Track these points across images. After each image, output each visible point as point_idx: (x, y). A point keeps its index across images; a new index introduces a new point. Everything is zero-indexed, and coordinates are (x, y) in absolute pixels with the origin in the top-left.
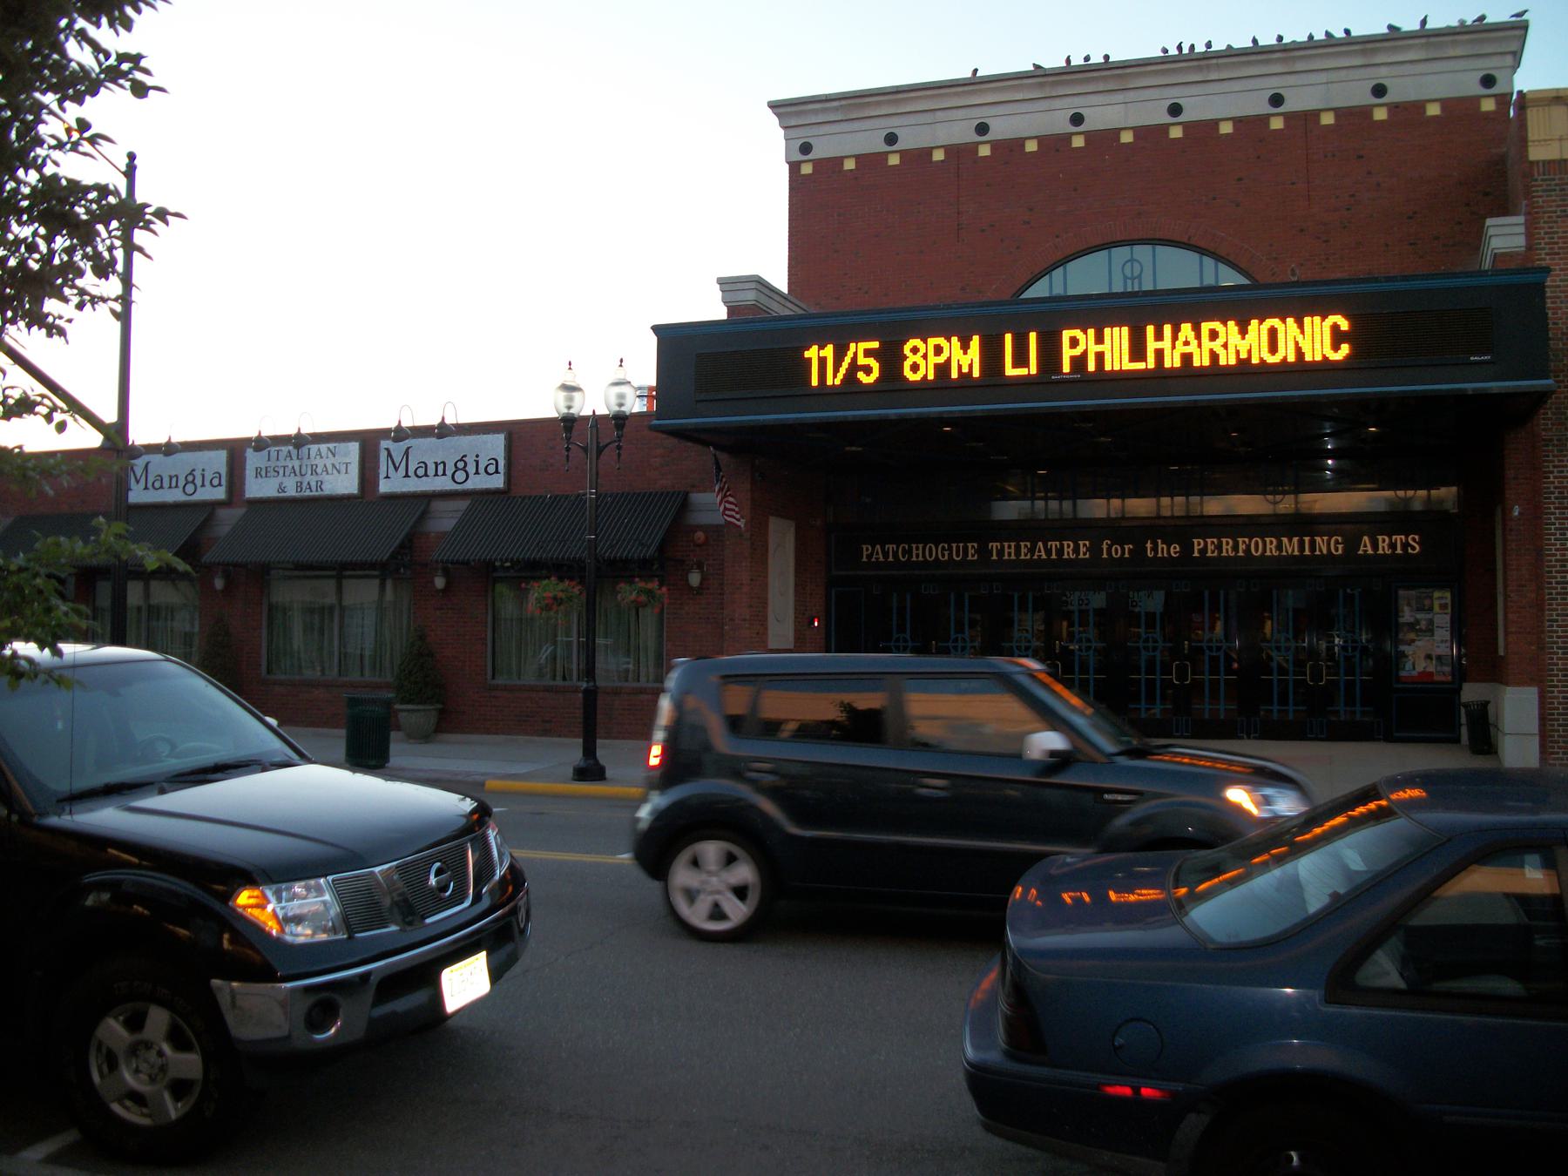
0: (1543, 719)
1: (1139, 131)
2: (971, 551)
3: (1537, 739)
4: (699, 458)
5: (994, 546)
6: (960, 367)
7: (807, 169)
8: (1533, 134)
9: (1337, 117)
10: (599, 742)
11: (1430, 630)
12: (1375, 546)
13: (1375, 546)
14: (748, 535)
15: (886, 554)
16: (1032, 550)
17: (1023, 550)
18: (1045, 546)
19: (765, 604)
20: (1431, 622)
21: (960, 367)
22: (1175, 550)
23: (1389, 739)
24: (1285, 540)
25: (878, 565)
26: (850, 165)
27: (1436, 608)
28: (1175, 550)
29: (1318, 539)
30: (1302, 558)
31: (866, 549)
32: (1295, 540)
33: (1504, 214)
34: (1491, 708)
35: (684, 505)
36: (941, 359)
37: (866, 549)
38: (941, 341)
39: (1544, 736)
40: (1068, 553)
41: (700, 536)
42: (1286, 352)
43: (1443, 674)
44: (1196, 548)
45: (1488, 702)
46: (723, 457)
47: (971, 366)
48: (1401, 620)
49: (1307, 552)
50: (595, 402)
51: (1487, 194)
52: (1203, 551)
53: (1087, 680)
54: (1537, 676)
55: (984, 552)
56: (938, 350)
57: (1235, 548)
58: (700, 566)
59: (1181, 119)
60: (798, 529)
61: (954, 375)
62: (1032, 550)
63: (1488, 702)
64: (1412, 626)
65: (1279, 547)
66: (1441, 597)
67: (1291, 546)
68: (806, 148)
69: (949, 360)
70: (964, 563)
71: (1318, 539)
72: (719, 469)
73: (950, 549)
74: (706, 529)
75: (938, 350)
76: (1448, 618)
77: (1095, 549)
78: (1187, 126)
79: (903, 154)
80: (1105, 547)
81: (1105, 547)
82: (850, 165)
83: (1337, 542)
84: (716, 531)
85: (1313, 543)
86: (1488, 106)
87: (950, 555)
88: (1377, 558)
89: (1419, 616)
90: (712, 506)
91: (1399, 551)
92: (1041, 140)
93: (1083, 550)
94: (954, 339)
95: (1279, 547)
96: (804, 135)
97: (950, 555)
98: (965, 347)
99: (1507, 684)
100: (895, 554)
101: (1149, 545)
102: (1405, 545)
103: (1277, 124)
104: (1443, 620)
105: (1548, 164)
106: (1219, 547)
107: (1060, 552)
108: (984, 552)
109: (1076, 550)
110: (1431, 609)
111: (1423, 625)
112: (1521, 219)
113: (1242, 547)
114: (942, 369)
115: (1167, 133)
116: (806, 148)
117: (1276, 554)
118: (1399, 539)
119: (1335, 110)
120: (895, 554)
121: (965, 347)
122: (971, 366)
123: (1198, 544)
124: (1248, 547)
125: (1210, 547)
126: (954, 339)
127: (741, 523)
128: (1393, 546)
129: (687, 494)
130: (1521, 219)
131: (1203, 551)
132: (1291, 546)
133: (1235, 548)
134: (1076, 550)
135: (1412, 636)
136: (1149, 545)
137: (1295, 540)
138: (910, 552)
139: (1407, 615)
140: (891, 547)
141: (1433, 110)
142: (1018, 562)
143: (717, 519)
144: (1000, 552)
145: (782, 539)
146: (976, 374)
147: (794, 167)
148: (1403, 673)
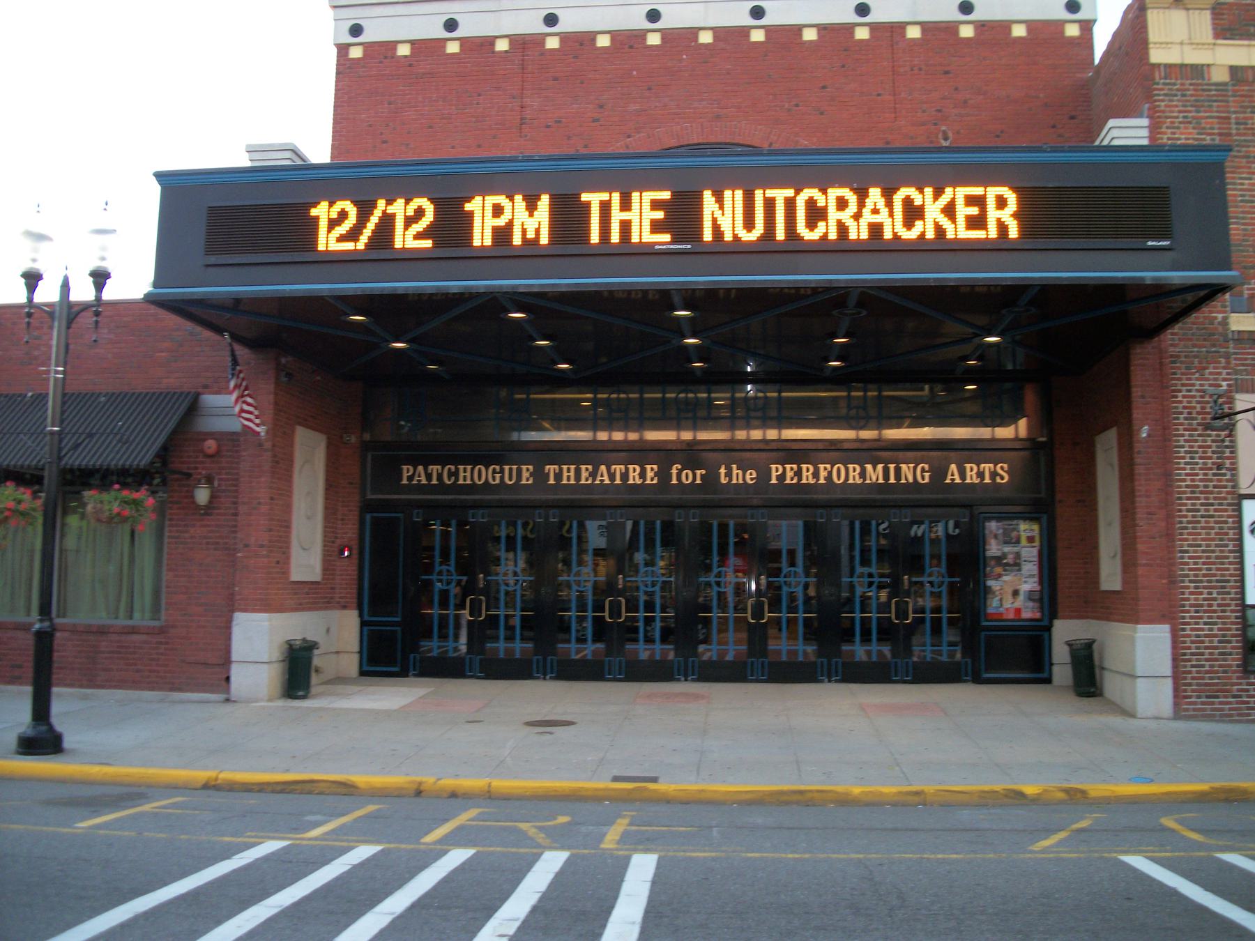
0: (1176, 660)
1: (718, 32)
2: (525, 475)
3: (1169, 684)
4: (212, 348)
5: (551, 469)
6: (524, 231)
7: (356, 53)
8: (1154, 35)
9: (924, 31)
10: (55, 690)
11: (1017, 565)
12: (962, 474)
13: (962, 474)
14: (268, 445)
15: (429, 476)
16: (593, 474)
17: (584, 474)
18: (608, 469)
19: (286, 526)
20: (1018, 555)
21: (524, 231)
22: (751, 476)
23: (978, 680)
24: (869, 467)
25: (420, 488)
26: (404, 50)
27: (1024, 542)
28: (751, 476)
29: (904, 467)
30: (885, 487)
31: (407, 470)
32: (880, 467)
33: (1124, 117)
34: (1095, 646)
35: (193, 408)
36: (501, 222)
37: (407, 470)
38: (502, 200)
39: (1177, 677)
40: (634, 478)
41: (211, 445)
42: (925, 228)
43: (1030, 612)
44: (774, 474)
45: (1094, 641)
46: (241, 351)
47: (538, 231)
48: (989, 554)
49: (892, 481)
50: (66, 275)
51: (1072, 118)
52: (782, 477)
53: (726, 619)
54: (1168, 613)
55: (539, 475)
56: (498, 211)
57: (816, 475)
58: (209, 480)
59: (763, 22)
60: (329, 445)
61: (517, 240)
62: (593, 474)
63: (1094, 641)
64: (999, 560)
65: (863, 474)
66: (1026, 529)
67: (875, 474)
68: (356, 30)
69: (510, 224)
70: (517, 486)
71: (904, 467)
72: (235, 362)
73: (502, 471)
74: (220, 437)
75: (498, 211)
76: (1035, 551)
77: (663, 474)
78: (769, 30)
79: (463, 41)
80: (674, 471)
81: (674, 471)
82: (404, 50)
83: (923, 470)
84: (231, 441)
85: (898, 471)
86: (1072, 31)
87: (502, 478)
88: (965, 487)
89: (1007, 549)
90: (230, 409)
91: (987, 480)
92: (614, 34)
93: (650, 474)
94: (518, 198)
95: (863, 474)
96: (354, 16)
97: (502, 478)
98: (531, 207)
99: (1137, 623)
100: (440, 476)
101: (723, 471)
102: (994, 475)
103: (862, 34)
104: (1030, 553)
105: (1169, 67)
106: (798, 473)
107: (625, 476)
108: (539, 475)
109: (643, 475)
110: (1018, 541)
111: (1010, 559)
112: (1145, 122)
113: (823, 474)
114: (502, 235)
115: (748, 36)
116: (356, 30)
117: (859, 481)
118: (987, 467)
119: (921, 24)
120: (440, 476)
121: (531, 207)
122: (538, 231)
123: (775, 470)
124: (830, 473)
125: (789, 474)
126: (518, 198)
127: (261, 430)
128: (981, 475)
129: (198, 395)
130: (1145, 122)
131: (782, 477)
132: (875, 474)
133: (816, 475)
134: (643, 475)
135: (999, 570)
136: (723, 471)
137: (880, 467)
138: (456, 474)
139: (993, 549)
140: (435, 469)
141: (1019, 31)
142: (578, 488)
143: (234, 425)
144: (558, 476)
145: (310, 457)
146: (544, 240)
147: (343, 49)
148: (990, 610)
